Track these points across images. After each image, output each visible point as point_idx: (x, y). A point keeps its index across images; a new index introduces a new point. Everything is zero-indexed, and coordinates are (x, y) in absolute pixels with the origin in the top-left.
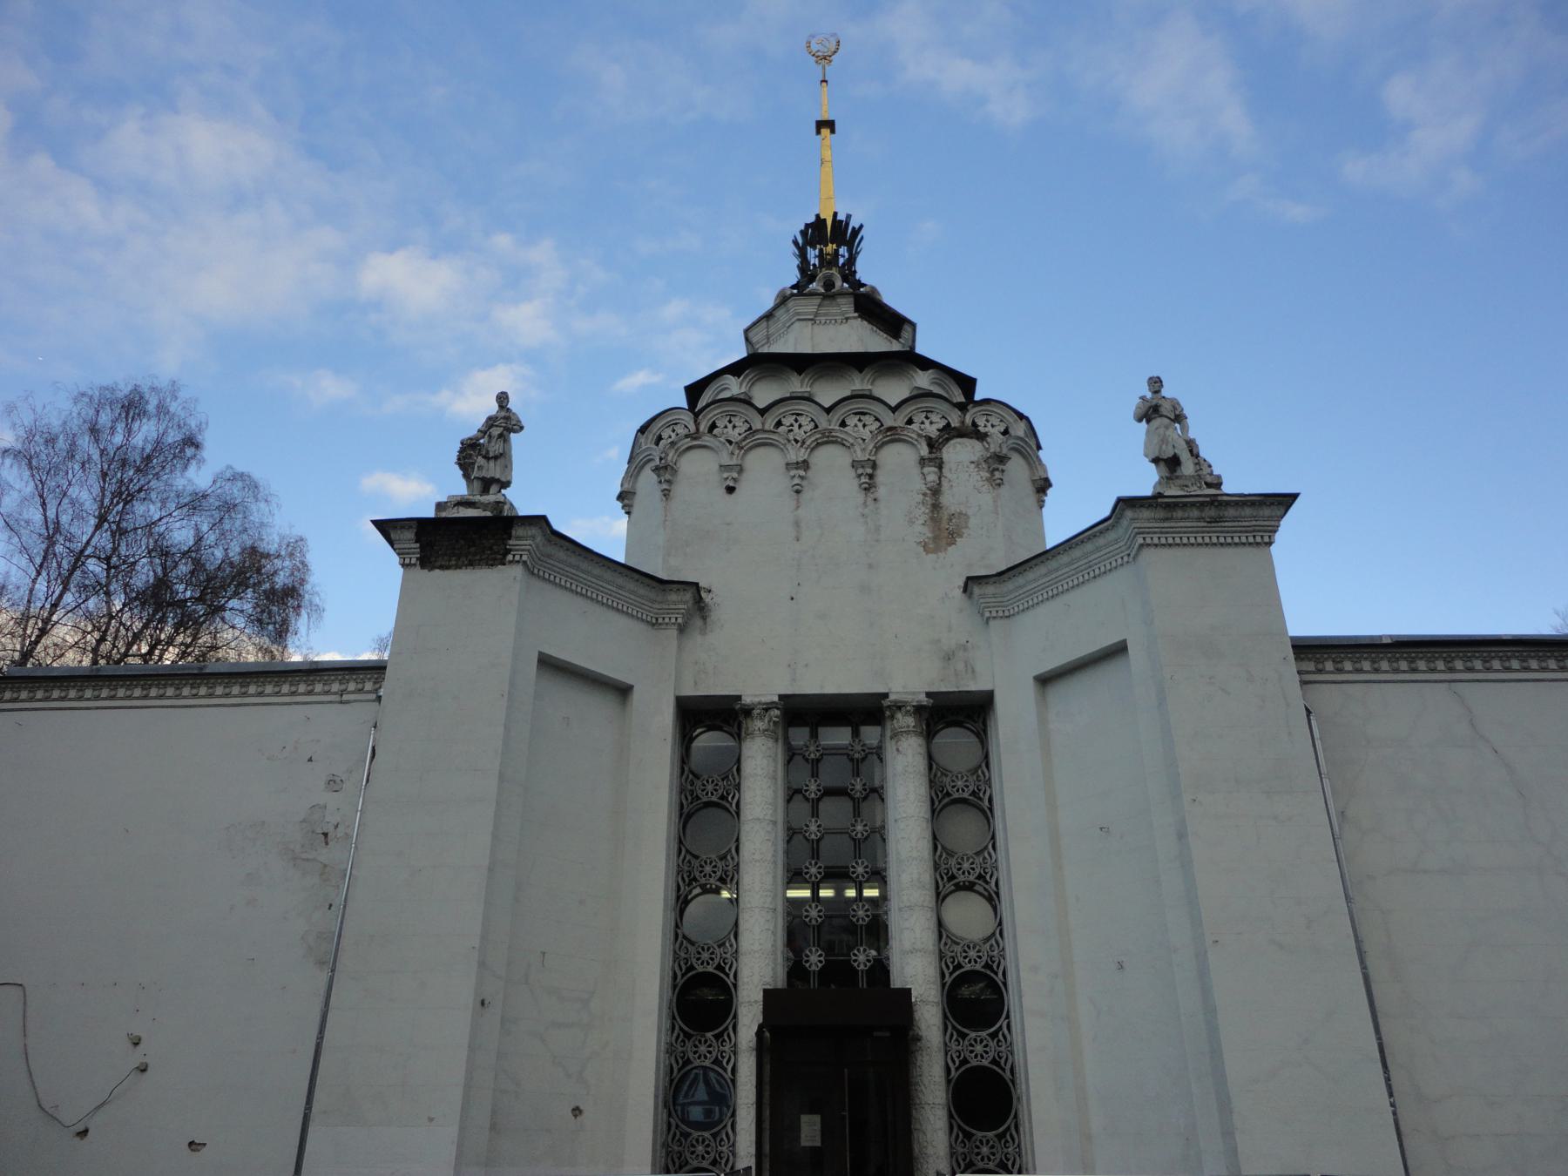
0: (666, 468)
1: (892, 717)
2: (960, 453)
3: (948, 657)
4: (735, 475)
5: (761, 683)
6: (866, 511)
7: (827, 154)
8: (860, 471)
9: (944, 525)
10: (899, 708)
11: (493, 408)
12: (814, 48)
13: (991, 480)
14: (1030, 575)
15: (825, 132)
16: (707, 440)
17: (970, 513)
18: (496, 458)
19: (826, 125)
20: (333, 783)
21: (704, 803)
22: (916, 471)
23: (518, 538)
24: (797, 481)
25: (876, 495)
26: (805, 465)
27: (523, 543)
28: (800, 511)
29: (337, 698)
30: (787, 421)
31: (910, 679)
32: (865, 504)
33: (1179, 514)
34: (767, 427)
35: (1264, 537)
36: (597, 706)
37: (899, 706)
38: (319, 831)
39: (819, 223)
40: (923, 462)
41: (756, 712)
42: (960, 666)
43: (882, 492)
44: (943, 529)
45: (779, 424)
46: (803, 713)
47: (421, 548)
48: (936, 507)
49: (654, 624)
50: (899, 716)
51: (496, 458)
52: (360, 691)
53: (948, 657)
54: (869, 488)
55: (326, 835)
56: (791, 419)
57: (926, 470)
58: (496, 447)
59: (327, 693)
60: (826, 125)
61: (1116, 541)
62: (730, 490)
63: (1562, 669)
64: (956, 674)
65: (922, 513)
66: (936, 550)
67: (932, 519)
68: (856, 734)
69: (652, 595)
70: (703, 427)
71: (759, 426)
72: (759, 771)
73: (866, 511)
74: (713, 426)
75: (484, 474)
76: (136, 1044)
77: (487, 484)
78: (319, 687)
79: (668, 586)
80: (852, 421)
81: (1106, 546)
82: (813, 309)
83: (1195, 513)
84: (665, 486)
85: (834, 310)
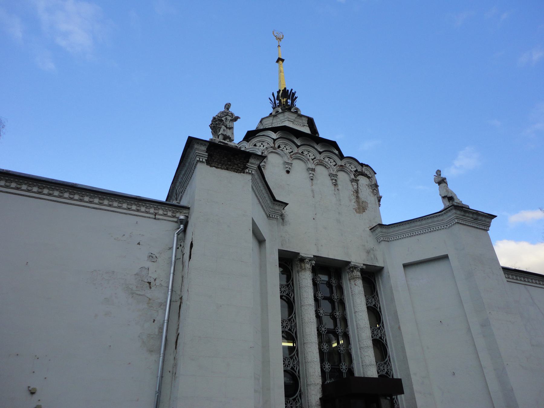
1: (353, 271)
2: (363, 180)
3: (368, 252)
5: (308, 251)
7: (282, 69)
8: (333, 178)
9: (361, 204)
11: (223, 109)
14: (401, 227)
15: (280, 62)
16: (278, 151)
19: (280, 60)
22: (350, 183)
23: (251, 163)
24: (311, 175)
28: (313, 187)
31: (358, 258)
33: (467, 215)
35: (486, 227)
37: (355, 267)
38: (146, 280)
40: (352, 181)
41: (306, 260)
42: (372, 256)
43: (340, 187)
44: (361, 207)
45: (302, 152)
48: (357, 197)
49: (269, 217)
54: (336, 185)
55: (150, 283)
57: (353, 183)
59: (147, 212)
60: (280, 60)
61: (442, 220)
62: (288, 172)
63: (543, 285)
65: (353, 198)
66: (359, 213)
68: (330, 278)
69: (270, 204)
70: (276, 146)
71: (296, 151)
74: (279, 147)
75: (225, 133)
76: (33, 393)
77: (226, 137)
79: (276, 203)
80: (327, 160)
81: (437, 221)
83: (471, 216)
85: (300, 121)
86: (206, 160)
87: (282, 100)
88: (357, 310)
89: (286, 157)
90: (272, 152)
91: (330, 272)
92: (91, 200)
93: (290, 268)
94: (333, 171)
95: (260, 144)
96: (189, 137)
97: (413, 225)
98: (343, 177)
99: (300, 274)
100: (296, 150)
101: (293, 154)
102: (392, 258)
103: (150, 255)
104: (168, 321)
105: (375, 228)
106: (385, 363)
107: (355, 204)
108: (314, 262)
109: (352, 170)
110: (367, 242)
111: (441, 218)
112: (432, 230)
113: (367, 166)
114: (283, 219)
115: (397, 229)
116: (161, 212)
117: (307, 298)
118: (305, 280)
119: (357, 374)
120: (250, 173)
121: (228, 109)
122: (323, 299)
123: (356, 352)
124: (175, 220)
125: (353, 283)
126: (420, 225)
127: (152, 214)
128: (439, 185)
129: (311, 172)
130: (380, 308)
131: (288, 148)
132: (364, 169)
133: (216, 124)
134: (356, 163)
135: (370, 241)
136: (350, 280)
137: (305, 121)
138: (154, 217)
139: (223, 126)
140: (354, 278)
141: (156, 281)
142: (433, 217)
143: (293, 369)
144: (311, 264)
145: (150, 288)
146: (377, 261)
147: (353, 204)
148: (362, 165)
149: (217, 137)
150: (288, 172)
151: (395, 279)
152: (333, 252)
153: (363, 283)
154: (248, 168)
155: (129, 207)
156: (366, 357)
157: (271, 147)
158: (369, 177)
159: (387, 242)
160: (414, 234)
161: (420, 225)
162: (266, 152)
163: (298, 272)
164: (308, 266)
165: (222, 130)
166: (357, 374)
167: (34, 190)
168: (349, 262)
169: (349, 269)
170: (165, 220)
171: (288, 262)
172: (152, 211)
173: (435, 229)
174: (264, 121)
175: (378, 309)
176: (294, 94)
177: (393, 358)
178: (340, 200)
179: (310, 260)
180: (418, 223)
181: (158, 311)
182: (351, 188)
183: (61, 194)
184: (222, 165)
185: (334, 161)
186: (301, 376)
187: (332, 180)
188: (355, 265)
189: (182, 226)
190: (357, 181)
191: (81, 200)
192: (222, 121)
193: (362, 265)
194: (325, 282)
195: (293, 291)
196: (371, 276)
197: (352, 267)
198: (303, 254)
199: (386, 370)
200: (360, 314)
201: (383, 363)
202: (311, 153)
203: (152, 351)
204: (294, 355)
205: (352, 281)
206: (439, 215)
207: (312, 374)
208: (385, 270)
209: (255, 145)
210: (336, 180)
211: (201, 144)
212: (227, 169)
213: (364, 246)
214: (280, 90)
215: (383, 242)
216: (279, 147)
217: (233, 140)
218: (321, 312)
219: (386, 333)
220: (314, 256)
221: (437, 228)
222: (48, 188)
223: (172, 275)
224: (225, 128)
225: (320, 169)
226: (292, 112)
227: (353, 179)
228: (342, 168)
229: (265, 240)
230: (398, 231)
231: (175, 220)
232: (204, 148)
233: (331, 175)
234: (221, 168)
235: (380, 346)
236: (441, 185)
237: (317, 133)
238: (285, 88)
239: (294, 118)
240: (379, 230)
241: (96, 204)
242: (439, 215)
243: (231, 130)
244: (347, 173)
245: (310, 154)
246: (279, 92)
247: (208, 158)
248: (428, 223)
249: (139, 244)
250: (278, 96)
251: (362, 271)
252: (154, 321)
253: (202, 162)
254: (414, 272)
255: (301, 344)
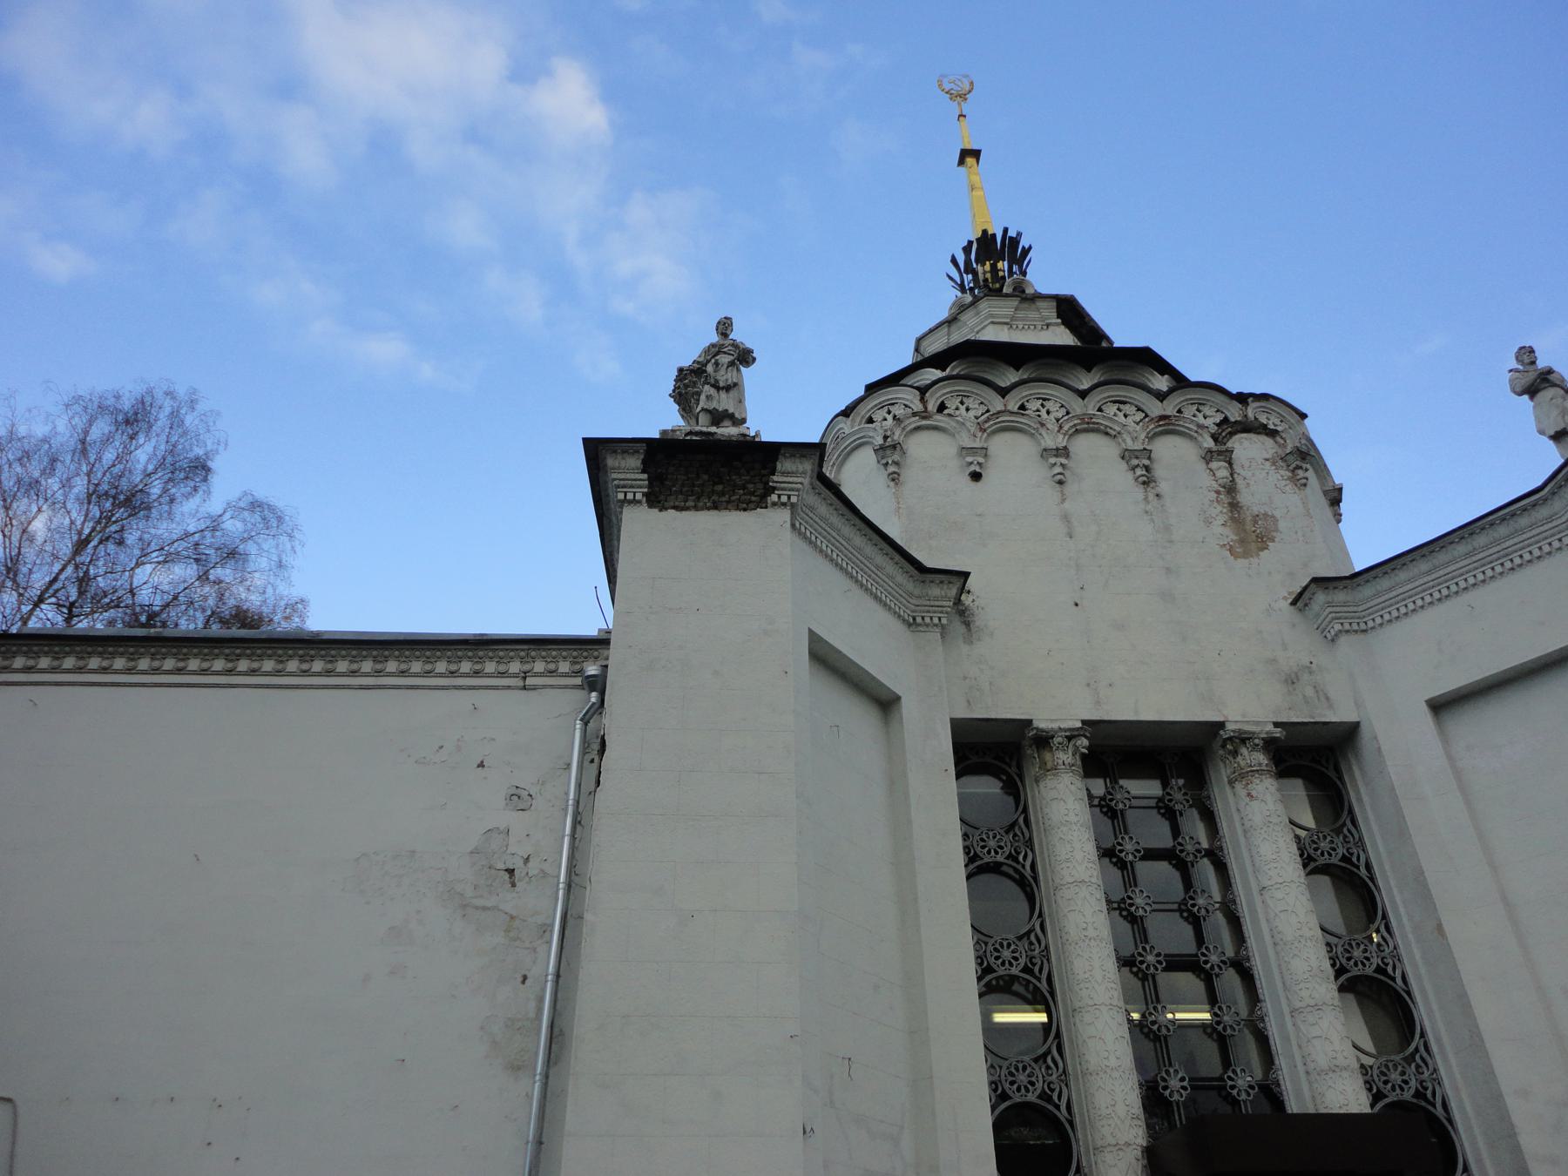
0: (894, 447)
1: (1235, 753)
2: (1247, 448)
3: (1292, 681)
4: (981, 460)
5: (1058, 705)
6: (1149, 507)
7: (975, 179)
8: (1135, 462)
9: (1249, 527)
10: (1243, 741)
12: (947, 86)
13: (1294, 479)
14: (1402, 575)
15: (970, 161)
16: (940, 420)
17: (1277, 514)
18: (728, 388)
19: (969, 155)
20: (518, 798)
21: (1003, 864)
22: (1201, 466)
23: (783, 473)
24: (1058, 469)
25: (1158, 490)
26: (1063, 452)
27: (793, 477)
28: (1066, 505)
29: (518, 682)
30: (1034, 405)
31: (1251, 705)
32: (1146, 499)
34: (1010, 408)
36: (858, 717)
37: (1243, 739)
38: (501, 866)
39: (986, 240)
40: (1209, 456)
41: (1057, 740)
42: (1309, 692)
43: (1164, 487)
44: (1251, 535)
45: (1022, 407)
46: (1115, 752)
47: (649, 479)
48: (1234, 506)
49: (912, 624)
50: (1244, 751)
51: (728, 388)
52: (552, 673)
53: (1292, 681)
54: (1148, 482)
55: (511, 872)
56: (1036, 405)
57: (1214, 465)
58: (724, 377)
59: (502, 674)
60: (969, 155)
61: (1550, 519)
62: (976, 476)
64: (1306, 700)
65: (1219, 513)
66: (1246, 554)
67: (1232, 519)
68: (1165, 785)
69: (910, 586)
70: (932, 406)
71: (1000, 407)
72: (1073, 818)
73: (1149, 507)
74: (942, 408)
75: (713, 405)
77: (718, 417)
78: (490, 667)
80: (1111, 410)
81: (1531, 526)
82: (1010, 312)
84: (892, 469)
85: (1032, 315)
86: (644, 494)
87: (980, 269)
88: (1266, 883)
89: (964, 434)
90: (918, 429)
91: (1157, 765)
92: (355, 667)
93: (1332, 774)
94: (1134, 439)
95: (883, 412)
96: (584, 440)
97: (1442, 557)
98: (1173, 454)
99: (1042, 785)
100: (997, 404)
101: (988, 420)
102: (1382, 687)
103: (514, 791)
104: (558, 976)
105: (1306, 595)
106: (1410, 1059)
107: (1227, 531)
108: (1085, 742)
109: (1209, 422)
110: (1285, 647)
111: (1543, 512)
112: (1517, 561)
113: (1265, 397)
114: (967, 624)
115: (1385, 583)
116: (539, 666)
117: (1067, 860)
118: (1064, 807)
119: (1293, 1107)
120: (784, 504)
121: (725, 335)
122: (1143, 858)
123: (1282, 1026)
124: (578, 681)
125: (1243, 793)
126: (1468, 555)
127: (515, 676)
128: (1532, 398)
129: (1053, 460)
130: (1368, 867)
131: (972, 405)
132: (1251, 412)
133: (686, 386)
134: (1220, 398)
135: (1296, 642)
136: (1231, 783)
137: (1049, 312)
138: (521, 683)
139: (707, 387)
140: (1242, 776)
141: (530, 864)
142: (1513, 515)
143: (1049, 1099)
144: (1076, 748)
145: (514, 885)
146: (1331, 707)
147: (1220, 530)
148: (1242, 398)
149: (693, 422)
150: (976, 476)
151: (1406, 765)
152: (1154, 699)
153: (1307, 789)
154: (774, 489)
155: (453, 667)
156: (1315, 1042)
157: (914, 414)
158: (1273, 433)
159: (1362, 636)
160: (1454, 588)
161: (1468, 555)
162: (897, 433)
163: (1037, 781)
164: (1064, 757)
165: (703, 397)
166: (1293, 1107)
167: (65, 666)
168: (1221, 725)
169: (1224, 746)
170: (552, 687)
171: (994, 752)
172: (515, 667)
173: (1527, 557)
174: (924, 343)
175: (1363, 872)
176: (1015, 242)
177: (1438, 1040)
178: (1167, 528)
179: (1069, 738)
180: (1461, 549)
181: (535, 950)
182: (1206, 481)
183: (280, 667)
184: (698, 499)
185: (1139, 409)
186: (1077, 1120)
187: (1133, 469)
188: (1240, 731)
189: (594, 697)
190: (1227, 456)
191: (328, 673)
192: (710, 375)
193: (1270, 727)
194: (1153, 803)
195: (1030, 843)
196: (1317, 758)
197: (1230, 739)
198: (1043, 722)
199: (1413, 1083)
200: (1279, 895)
201: (1397, 1058)
202: (1054, 402)
203: (519, 1068)
204: (1417, 1050)
205: (1238, 786)
206: (1534, 505)
207: (1104, 1112)
208: (1365, 732)
209: (870, 421)
210: (1147, 468)
211: (624, 452)
212: (715, 507)
213: (1274, 661)
214: (970, 243)
215: (1343, 639)
216: (942, 408)
217: (744, 421)
218: (1139, 901)
219: (1402, 950)
220: (1084, 722)
221: (1537, 553)
222: (249, 657)
223: (567, 840)
224: (713, 391)
225: (1087, 447)
226: (1007, 295)
227: (1210, 451)
228: (1166, 426)
229: (898, 698)
230: (1390, 589)
231: (578, 681)
232: (635, 462)
233: (1126, 455)
234: (696, 508)
235: (1379, 994)
236: (1541, 396)
237: (1102, 336)
238: (985, 232)
239: (1010, 312)
240: (1321, 597)
241: (367, 675)
242: (1534, 505)
243: (733, 393)
244: (1191, 437)
245: (1049, 405)
246: (967, 250)
247: (650, 486)
248: (1496, 542)
249: (481, 765)
250: (968, 262)
251: (1272, 746)
252: (525, 978)
253: (634, 502)
254: (1471, 725)
255: (1066, 1016)
